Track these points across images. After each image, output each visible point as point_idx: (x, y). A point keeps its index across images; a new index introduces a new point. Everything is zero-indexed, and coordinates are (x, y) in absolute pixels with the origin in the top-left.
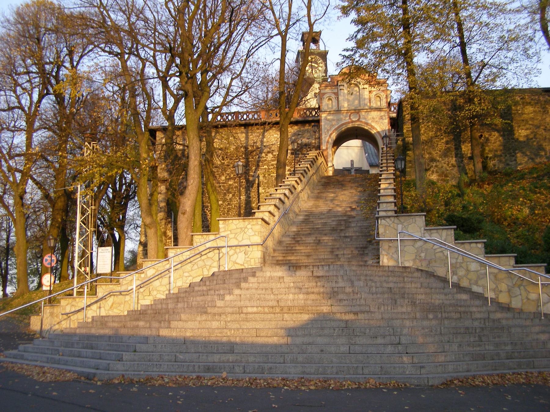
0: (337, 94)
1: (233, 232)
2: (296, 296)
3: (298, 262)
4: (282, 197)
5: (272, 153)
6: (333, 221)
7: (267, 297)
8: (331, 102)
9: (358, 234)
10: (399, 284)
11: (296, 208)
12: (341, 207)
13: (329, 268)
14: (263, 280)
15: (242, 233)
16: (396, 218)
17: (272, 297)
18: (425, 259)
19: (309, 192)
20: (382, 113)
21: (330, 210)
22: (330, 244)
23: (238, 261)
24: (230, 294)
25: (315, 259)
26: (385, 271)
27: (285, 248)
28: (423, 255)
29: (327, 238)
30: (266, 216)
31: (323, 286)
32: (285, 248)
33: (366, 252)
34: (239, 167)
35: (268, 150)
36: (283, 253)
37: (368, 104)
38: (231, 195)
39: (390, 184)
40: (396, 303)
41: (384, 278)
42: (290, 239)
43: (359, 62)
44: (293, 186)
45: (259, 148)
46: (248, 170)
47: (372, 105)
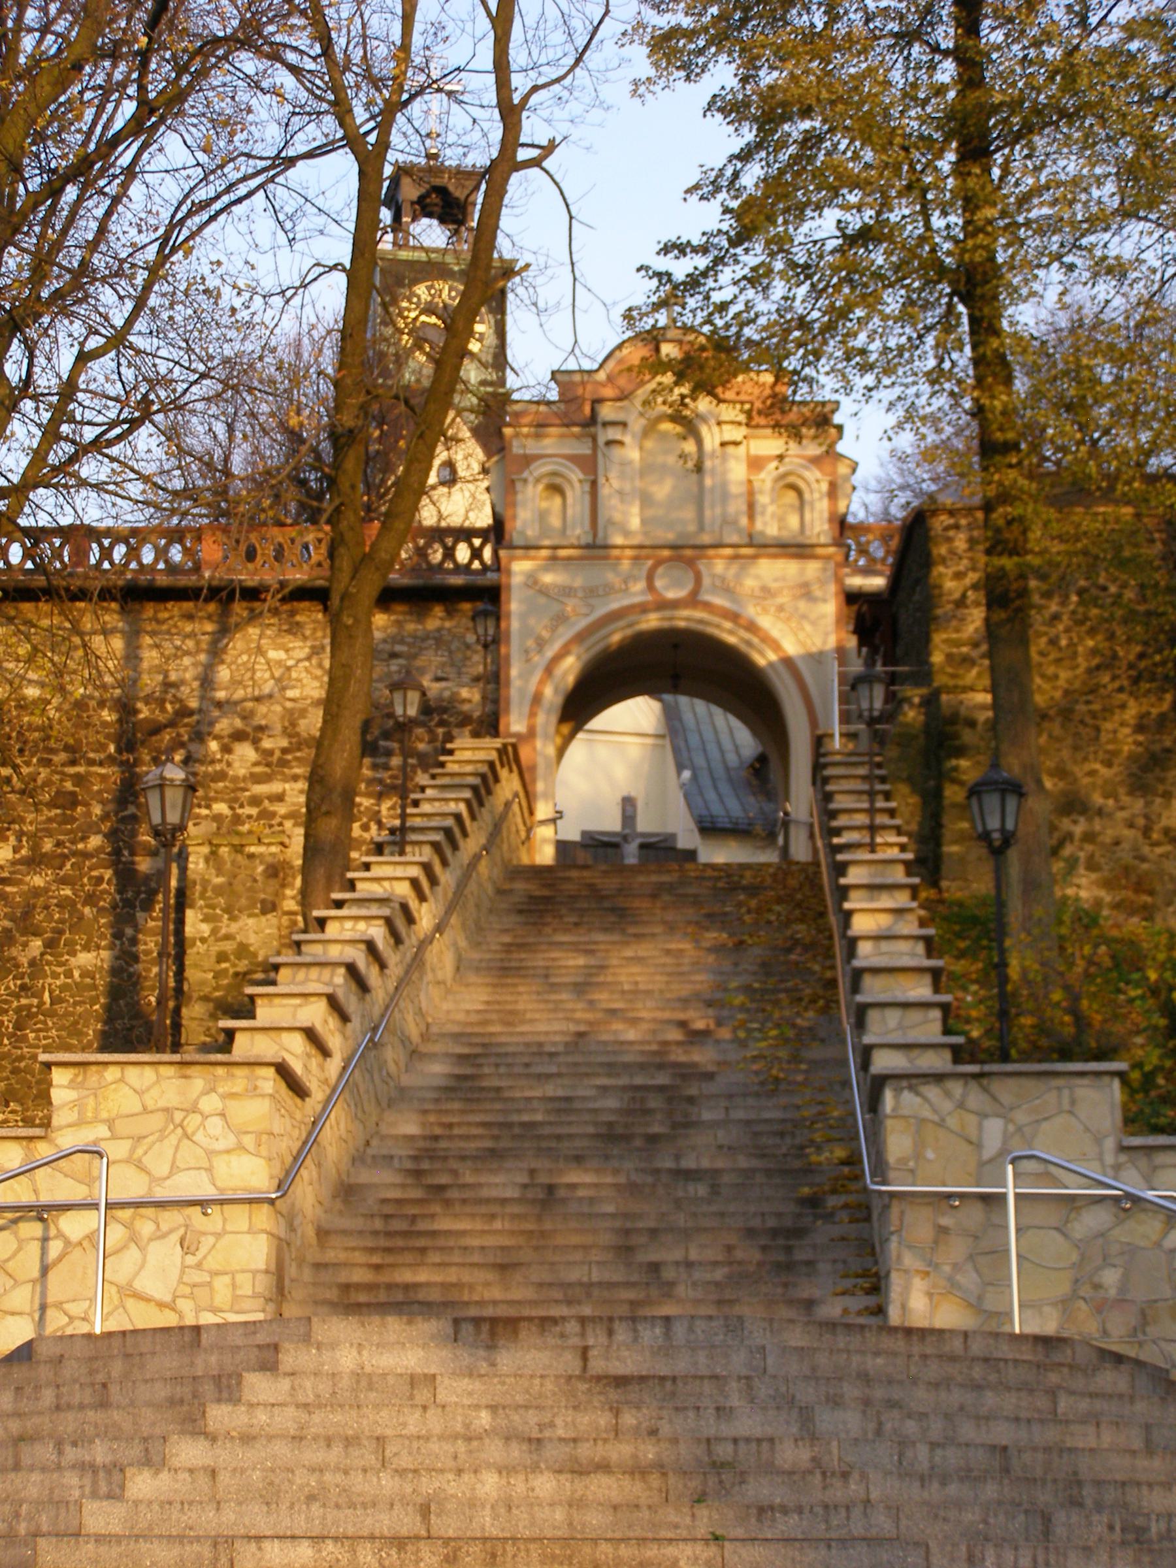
0: (590, 466)
1: (122, 1127)
2: (519, 1485)
3: (454, 1296)
4: (358, 956)
5: (256, 742)
6: (604, 1089)
7: (358, 1483)
8: (557, 501)
9: (743, 1162)
10: (1036, 1428)
11: (410, 1018)
12: (634, 1021)
13: (667, 1334)
14: (324, 1388)
15: (173, 1139)
16: (973, 1085)
17: (387, 1483)
18: (1121, 1301)
19: (463, 943)
20: (812, 568)
21: (581, 1035)
22: (610, 1209)
23: (141, 1284)
24: (147, 1462)
25: (541, 1285)
26: (953, 1359)
27: (378, 1224)
28: (1110, 1278)
29: (589, 1178)
30: (294, 1049)
31: (653, 1432)
32: (378, 1224)
33: (799, 1256)
34: (169, 793)
35: (238, 723)
36: (372, 1250)
37: (744, 521)
38: (37, 944)
39: (898, 912)
40: (1047, 1533)
41: (956, 1397)
42: (398, 1179)
43: (733, 310)
44: (405, 908)
45: (191, 713)
46: (134, 818)
47: (759, 525)
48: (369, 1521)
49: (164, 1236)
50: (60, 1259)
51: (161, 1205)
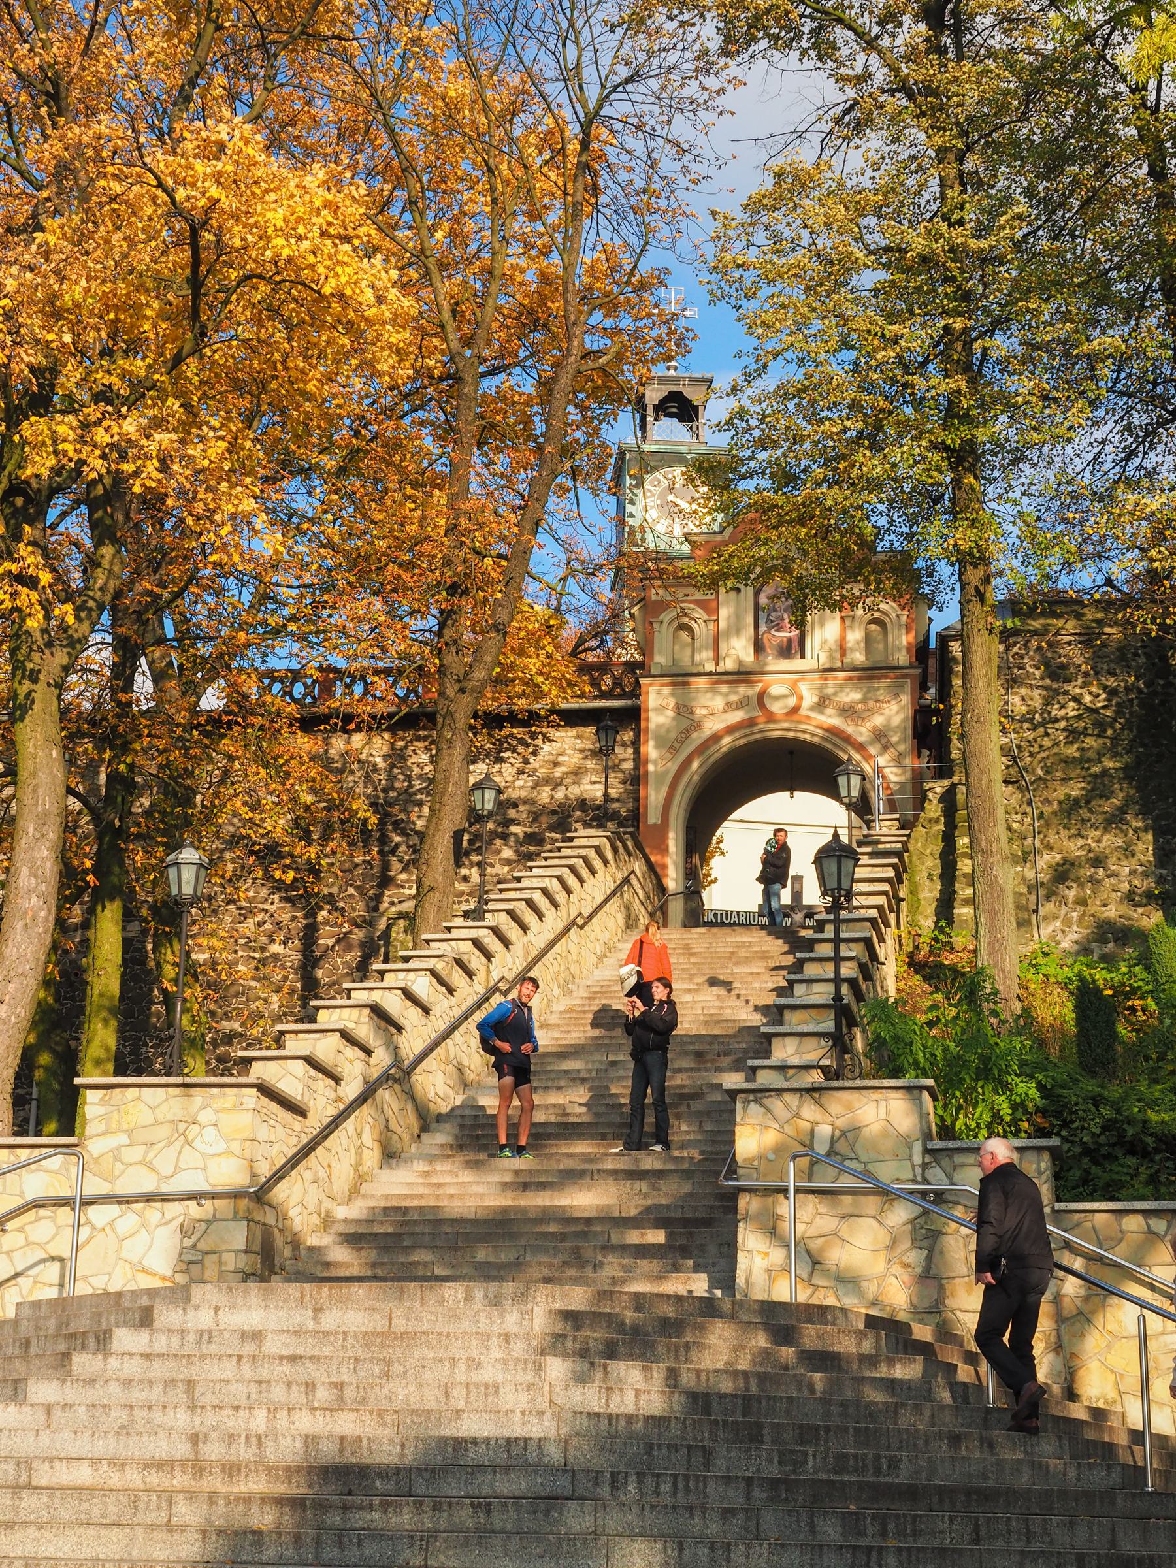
16: (807, 1097)
48: (152, 1446)
49: (167, 1223)
50: (88, 1241)
51: (166, 1198)
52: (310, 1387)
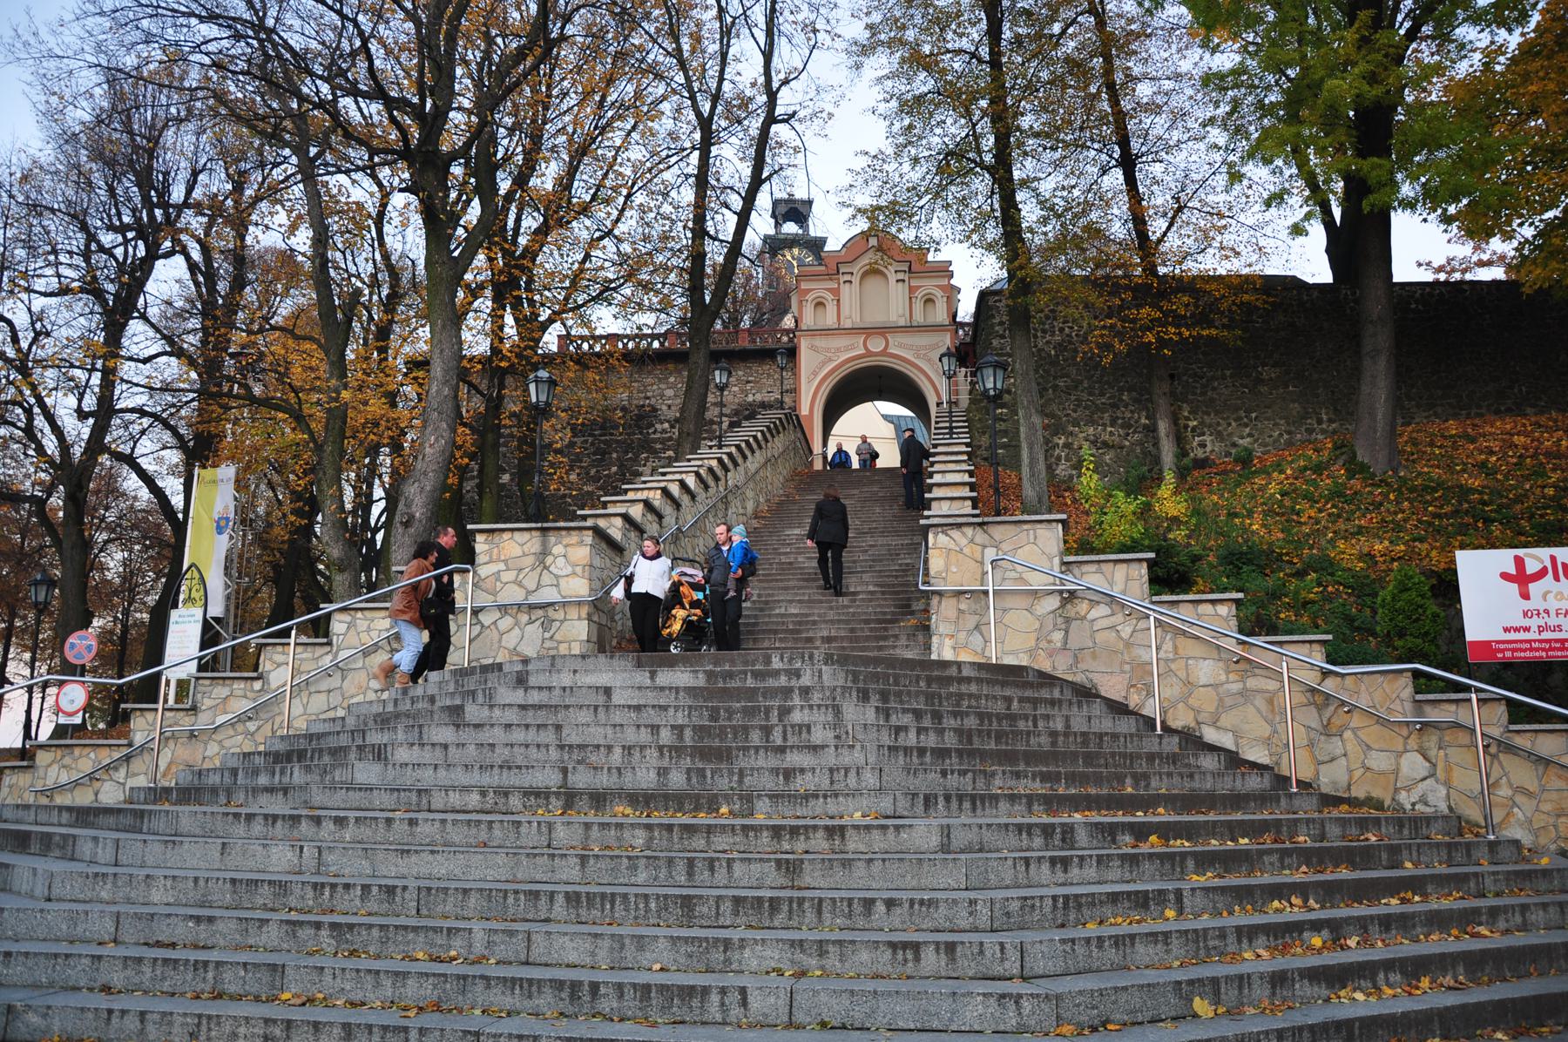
52: (655, 729)
